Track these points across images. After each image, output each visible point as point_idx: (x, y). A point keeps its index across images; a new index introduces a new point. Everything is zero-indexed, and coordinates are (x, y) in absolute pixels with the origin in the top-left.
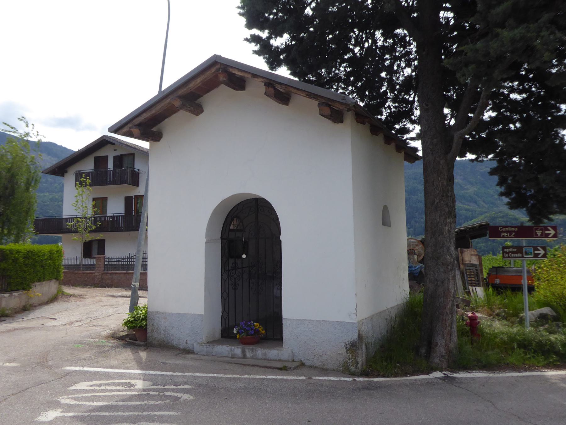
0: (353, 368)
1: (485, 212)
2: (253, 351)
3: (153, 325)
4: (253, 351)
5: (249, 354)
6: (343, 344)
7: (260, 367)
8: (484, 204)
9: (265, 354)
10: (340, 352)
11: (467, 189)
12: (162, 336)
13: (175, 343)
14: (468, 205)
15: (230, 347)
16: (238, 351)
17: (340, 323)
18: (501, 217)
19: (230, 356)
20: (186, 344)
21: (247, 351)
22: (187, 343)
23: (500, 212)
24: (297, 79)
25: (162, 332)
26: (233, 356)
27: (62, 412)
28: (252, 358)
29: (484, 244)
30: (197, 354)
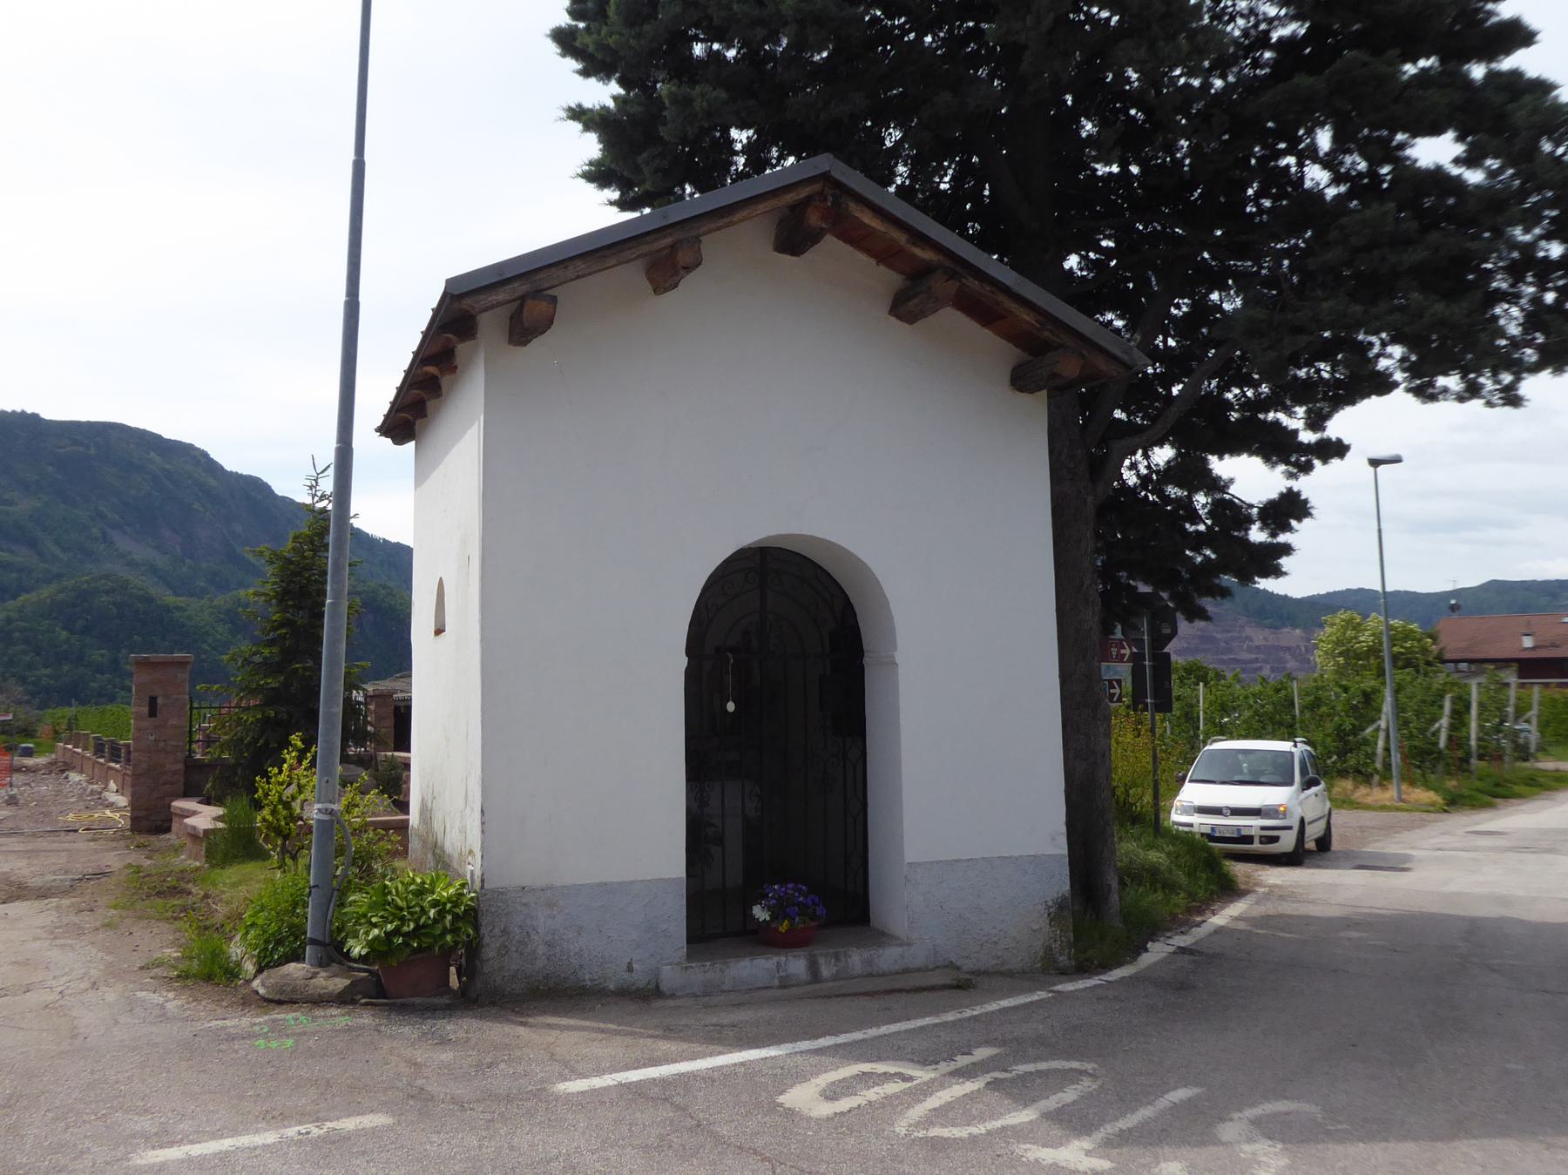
0: (1063, 960)
1: (59, 577)
2: (837, 959)
3: (505, 931)
4: (837, 959)
5: (826, 970)
6: (1041, 908)
7: (908, 991)
8: (56, 550)
9: (869, 962)
10: (1036, 927)
11: (11, 503)
12: (539, 964)
13: (587, 977)
14: (12, 552)
15: (776, 959)
16: (797, 965)
17: (1034, 859)
18: (108, 592)
19: (776, 982)
20: (626, 976)
21: (822, 961)
22: (630, 969)
23: (106, 577)
24: (647, 211)
25: (541, 950)
26: (785, 984)
27: (1088, 1153)
28: (835, 978)
29: (48, 671)
30: (673, 996)
